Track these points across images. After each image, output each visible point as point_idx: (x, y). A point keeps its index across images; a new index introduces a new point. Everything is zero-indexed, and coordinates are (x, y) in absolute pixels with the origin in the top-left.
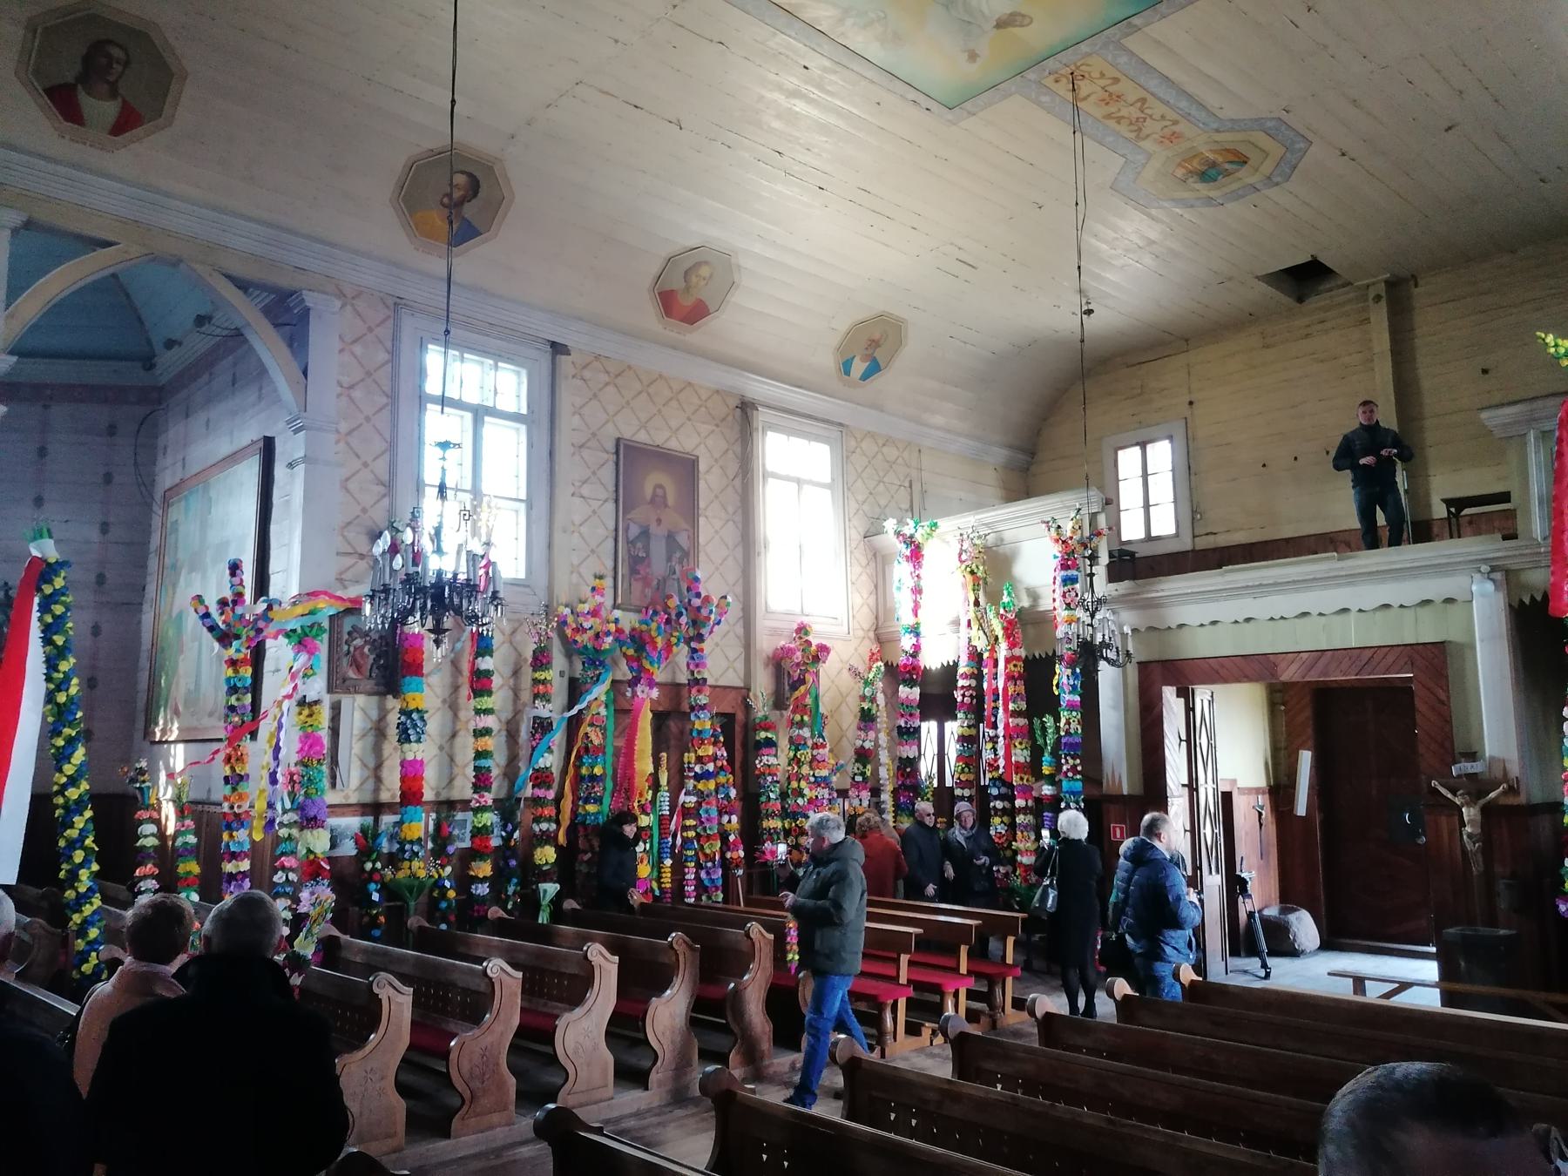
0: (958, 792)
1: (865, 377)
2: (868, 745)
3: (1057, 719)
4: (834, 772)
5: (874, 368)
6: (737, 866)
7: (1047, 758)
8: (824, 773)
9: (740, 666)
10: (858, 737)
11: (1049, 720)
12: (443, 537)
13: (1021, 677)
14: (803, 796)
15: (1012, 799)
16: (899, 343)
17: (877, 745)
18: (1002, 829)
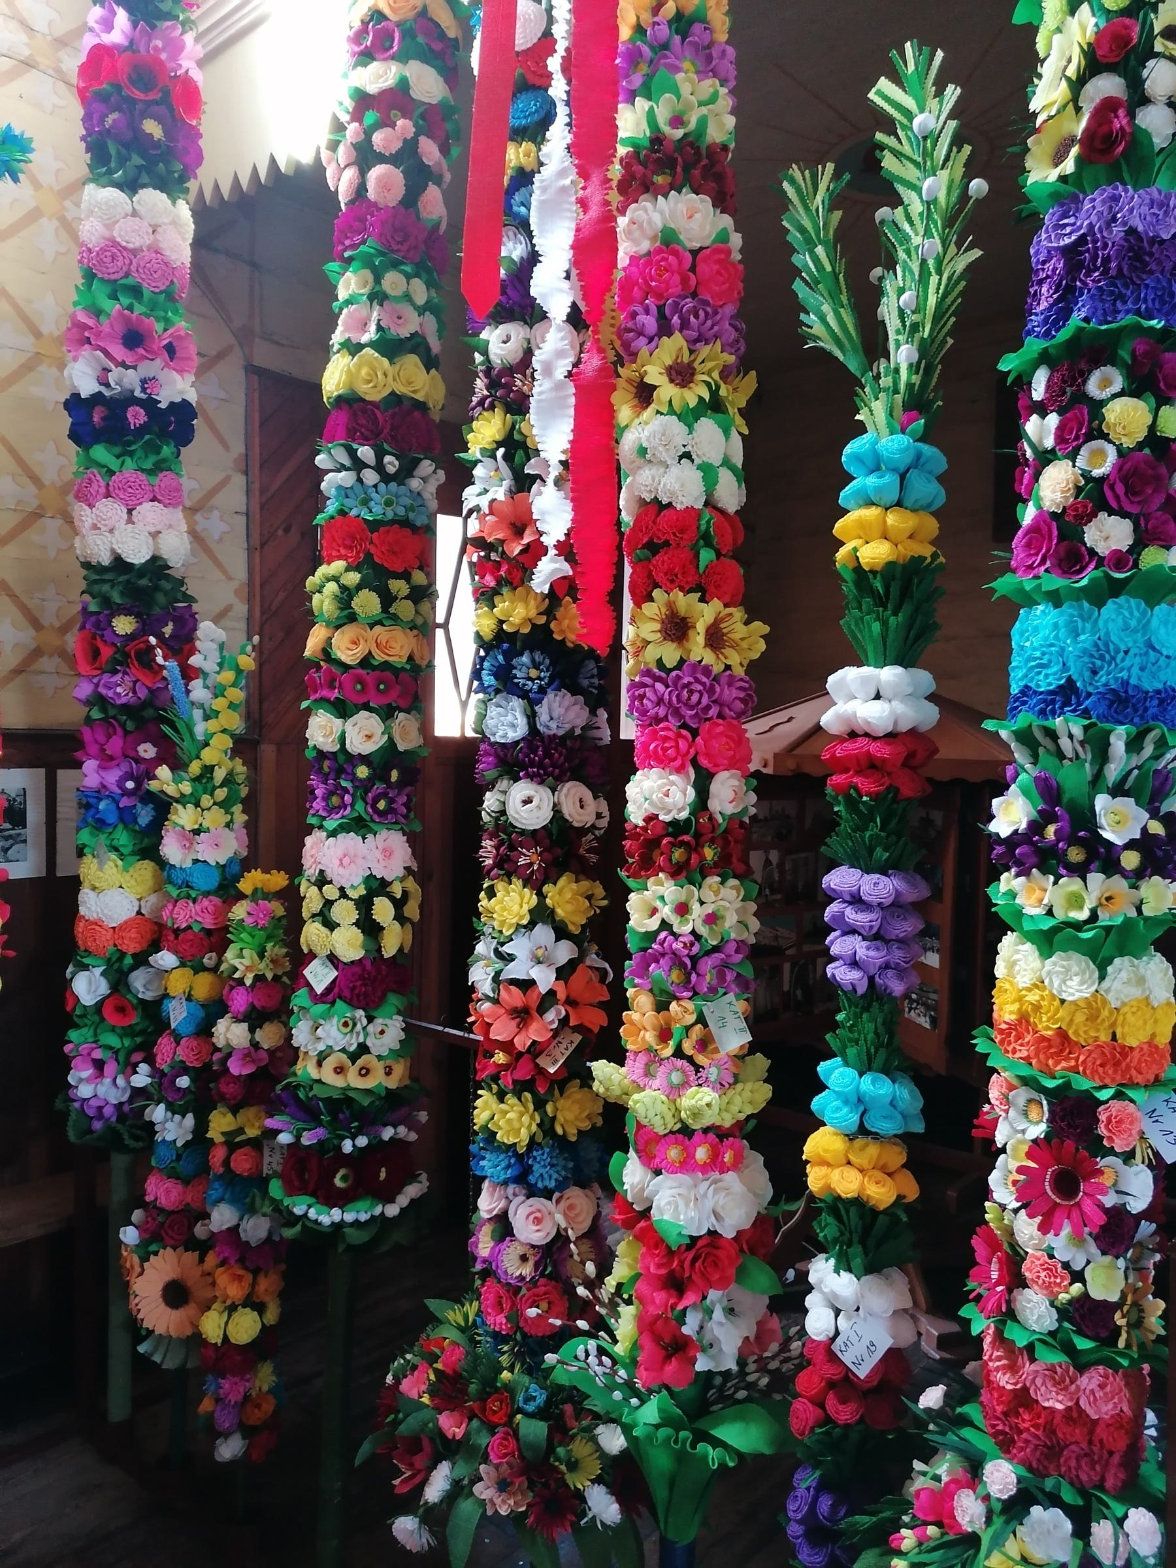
7: (881, 437)
12: (450, 626)
15: (609, 769)
18: (535, 959)
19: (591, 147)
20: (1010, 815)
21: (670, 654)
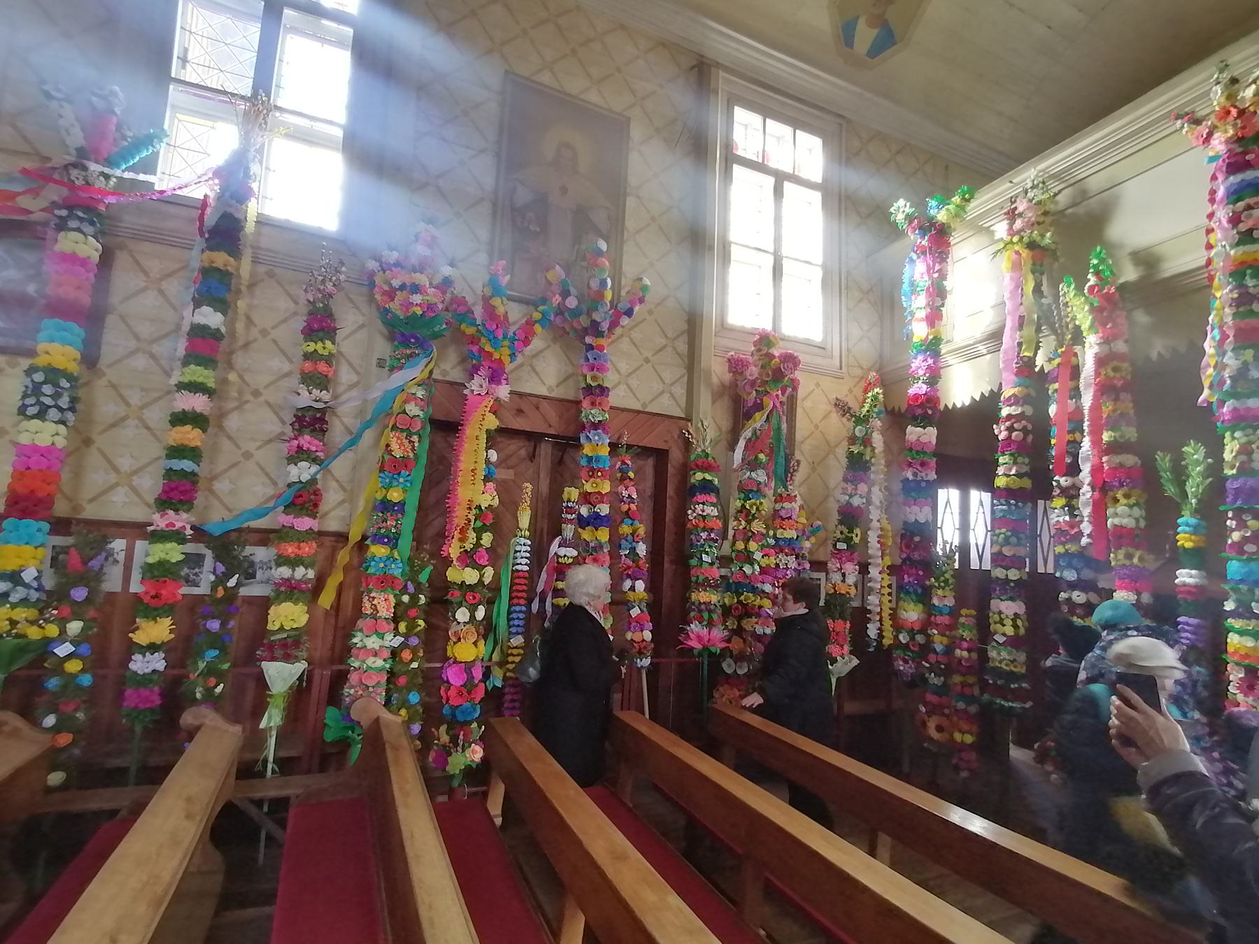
0: (728, 666)
2: (856, 501)
3: (1215, 449)
5: (887, 40)
6: (641, 654)
7: (1187, 520)
8: (791, 534)
9: (680, 391)
11: (1195, 453)
13: (1127, 387)
17: (869, 502)
19: (1096, 442)
20: (1229, 606)
21: (1127, 563)
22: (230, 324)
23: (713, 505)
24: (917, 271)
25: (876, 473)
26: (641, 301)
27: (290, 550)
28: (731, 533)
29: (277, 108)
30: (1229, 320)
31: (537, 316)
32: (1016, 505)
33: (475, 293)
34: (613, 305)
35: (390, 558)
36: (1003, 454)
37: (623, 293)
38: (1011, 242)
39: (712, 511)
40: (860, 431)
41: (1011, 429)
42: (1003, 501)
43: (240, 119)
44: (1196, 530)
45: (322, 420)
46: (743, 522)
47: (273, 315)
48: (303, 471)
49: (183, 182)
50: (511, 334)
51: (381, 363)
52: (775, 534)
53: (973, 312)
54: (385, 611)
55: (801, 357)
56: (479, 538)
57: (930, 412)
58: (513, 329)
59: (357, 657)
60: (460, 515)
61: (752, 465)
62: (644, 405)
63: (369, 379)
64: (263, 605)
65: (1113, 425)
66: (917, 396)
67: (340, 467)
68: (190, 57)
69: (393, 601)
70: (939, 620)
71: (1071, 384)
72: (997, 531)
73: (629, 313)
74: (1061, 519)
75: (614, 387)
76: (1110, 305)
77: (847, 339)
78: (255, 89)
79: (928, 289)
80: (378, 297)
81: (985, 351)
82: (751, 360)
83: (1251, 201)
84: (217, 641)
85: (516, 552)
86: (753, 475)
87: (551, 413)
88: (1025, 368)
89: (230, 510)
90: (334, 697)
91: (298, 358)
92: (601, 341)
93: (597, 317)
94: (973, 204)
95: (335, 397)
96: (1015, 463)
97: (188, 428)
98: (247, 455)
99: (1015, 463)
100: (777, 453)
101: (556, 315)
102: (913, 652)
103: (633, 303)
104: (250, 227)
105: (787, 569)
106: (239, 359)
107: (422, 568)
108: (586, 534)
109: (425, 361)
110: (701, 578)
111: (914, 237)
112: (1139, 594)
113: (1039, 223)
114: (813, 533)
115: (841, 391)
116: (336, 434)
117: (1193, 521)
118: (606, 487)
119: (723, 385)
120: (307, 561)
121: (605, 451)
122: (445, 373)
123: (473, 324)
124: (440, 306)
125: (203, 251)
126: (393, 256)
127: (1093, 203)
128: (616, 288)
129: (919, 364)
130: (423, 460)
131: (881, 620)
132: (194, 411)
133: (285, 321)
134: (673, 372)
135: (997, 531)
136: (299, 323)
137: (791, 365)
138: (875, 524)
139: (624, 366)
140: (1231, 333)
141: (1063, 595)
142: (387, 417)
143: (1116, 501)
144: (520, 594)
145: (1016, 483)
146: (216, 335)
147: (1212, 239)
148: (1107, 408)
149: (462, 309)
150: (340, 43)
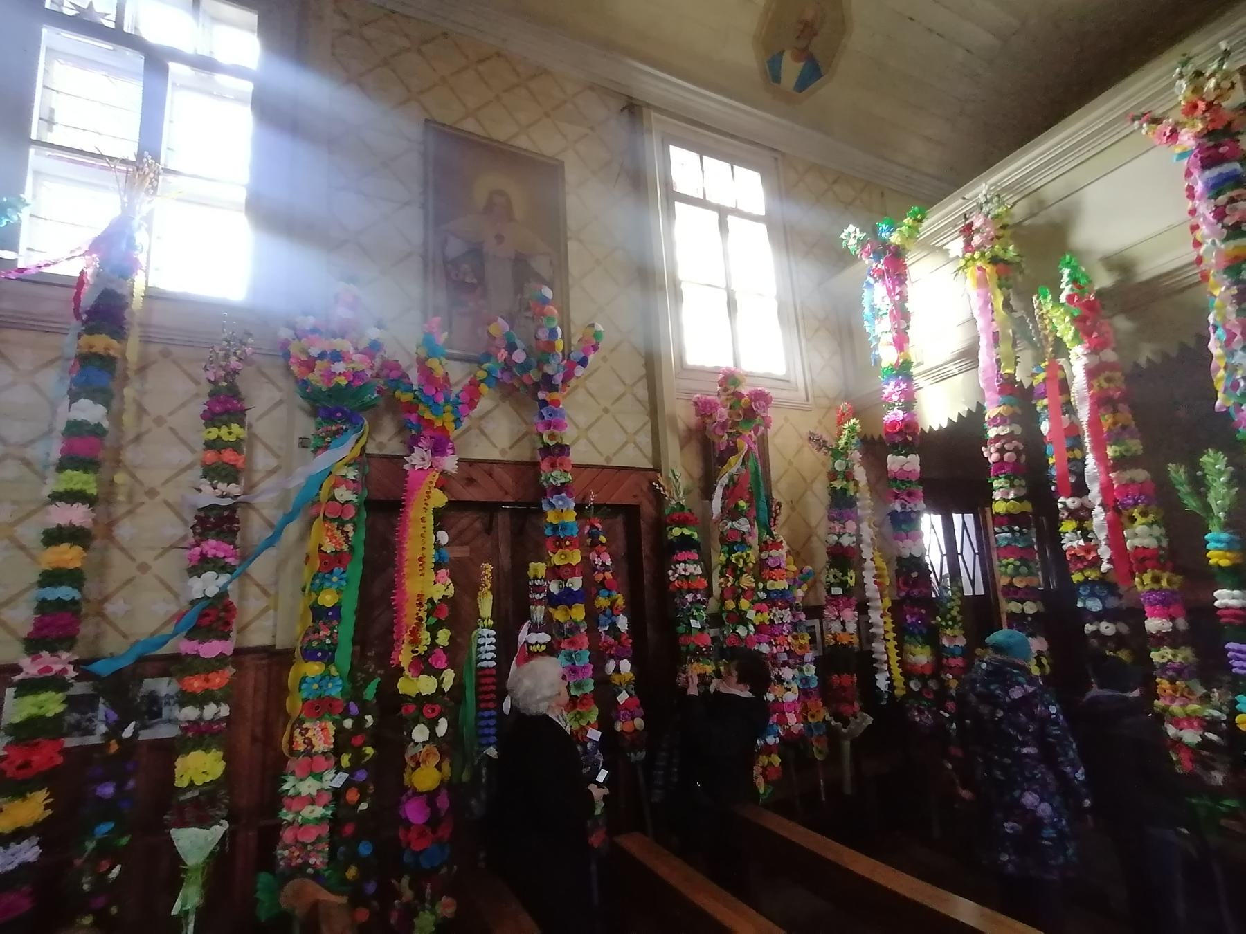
1: (803, 84)
2: (846, 541)
4: (796, 583)
5: (813, 73)
8: (782, 584)
9: (645, 440)
10: (831, 532)
14: (744, 621)
16: (842, 27)
17: (859, 541)
19: (1101, 458)
21: (1156, 587)
22: (115, 417)
23: (695, 562)
24: (877, 295)
25: (863, 508)
26: (595, 348)
27: (196, 684)
28: (716, 591)
29: (167, 171)
30: (1233, 317)
31: (482, 375)
32: (1020, 532)
33: (409, 354)
34: (566, 355)
35: (326, 677)
36: (998, 478)
37: (574, 341)
38: (973, 259)
39: (695, 569)
40: (840, 465)
41: (1001, 451)
42: (1005, 528)
43: (122, 184)
44: (1230, 546)
45: (232, 519)
46: (731, 579)
47: (168, 404)
48: (209, 584)
49: (51, 258)
50: (453, 396)
51: (304, 443)
52: (765, 587)
53: (944, 333)
54: (322, 744)
55: (773, 393)
56: (434, 637)
57: (910, 438)
58: (456, 390)
59: (289, 809)
60: (411, 613)
61: (731, 512)
62: (608, 459)
63: (288, 464)
64: (169, 751)
65: (1115, 438)
66: (894, 424)
67: (261, 568)
68: (57, 118)
69: (331, 728)
70: (953, 662)
71: (1062, 399)
72: (1005, 562)
73: (583, 362)
74: (1075, 544)
75: (574, 442)
76: (1091, 315)
77: (810, 370)
78: (140, 156)
79: (891, 312)
80: (294, 368)
81: (956, 371)
82: (718, 401)
83: (1234, 193)
84: (107, 810)
85: (479, 646)
86: (735, 524)
87: (507, 479)
88: (1008, 387)
89: (125, 636)
90: (266, 860)
91: (200, 447)
92: (556, 395)
93: (549, 370)
94: (925, 223)
95: (250, 488)
96: (1012, 486)
97: (65, 546)
98: (144, 568)
99: (1012, 486)
100: (754, 494)
101: (503, 371)
102: (928, 700)
103: (586, 351)
104: (137, 303)
105: (783, 624)
106: (130, 455)
107: (367, 682)
108: (559, 615)
109: (354, 437)
110: (692, 647)
111: (868, 262)
112: (1172, 619)
113: (998, 238)
114: (804, 580)
115: (809, 424)
116: (255, 528)
117: (1225, 536)
118: (576, 558)
119: (689, 430)
120: (219, 694)
121: (571, 517)
122: (381, 446)
123: (411, 390)
124: (369, 373)
125: (79, 336)
126: (310, 322)
127: (1053, 213)
128: (567, 338)
129: (890, 389)
130: (360, 552)
131: (889, 669)
132: (72, 526)
133: (183, 405)
134: (636, 420)
135: (1005, 562)
136: (199, 407)
137: (763, 403)
138: (869, 564)
139: (581, 419)
140: (1238, 332)
141: (1089, 628)
142: (312, 506)
143: (1133, 520)
144: (488, 697)
145: (1016, 508)
146: (97, 431)
147: (1199, 235)
148: (1107, 420)
149: (394, 374)
150: (238, 100)
